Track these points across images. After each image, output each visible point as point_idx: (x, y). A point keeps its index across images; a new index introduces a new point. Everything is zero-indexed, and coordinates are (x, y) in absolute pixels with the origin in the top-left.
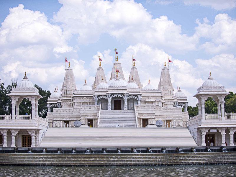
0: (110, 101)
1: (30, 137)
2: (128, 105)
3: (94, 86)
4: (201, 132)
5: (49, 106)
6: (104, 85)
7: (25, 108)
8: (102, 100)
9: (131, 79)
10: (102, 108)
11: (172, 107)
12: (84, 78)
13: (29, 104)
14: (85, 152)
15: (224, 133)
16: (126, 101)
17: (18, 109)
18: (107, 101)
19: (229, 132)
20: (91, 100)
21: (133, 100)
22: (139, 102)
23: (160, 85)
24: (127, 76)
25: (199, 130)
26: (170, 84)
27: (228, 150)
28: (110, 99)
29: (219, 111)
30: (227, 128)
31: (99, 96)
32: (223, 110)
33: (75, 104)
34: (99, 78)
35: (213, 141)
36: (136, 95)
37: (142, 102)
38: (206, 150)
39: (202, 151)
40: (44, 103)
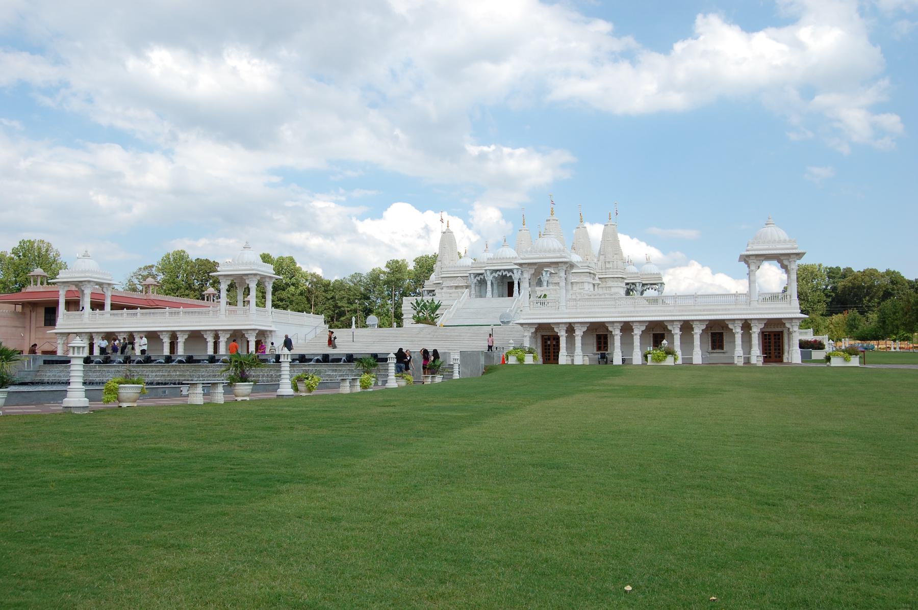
0: (489, 283)
31: (496, 271)
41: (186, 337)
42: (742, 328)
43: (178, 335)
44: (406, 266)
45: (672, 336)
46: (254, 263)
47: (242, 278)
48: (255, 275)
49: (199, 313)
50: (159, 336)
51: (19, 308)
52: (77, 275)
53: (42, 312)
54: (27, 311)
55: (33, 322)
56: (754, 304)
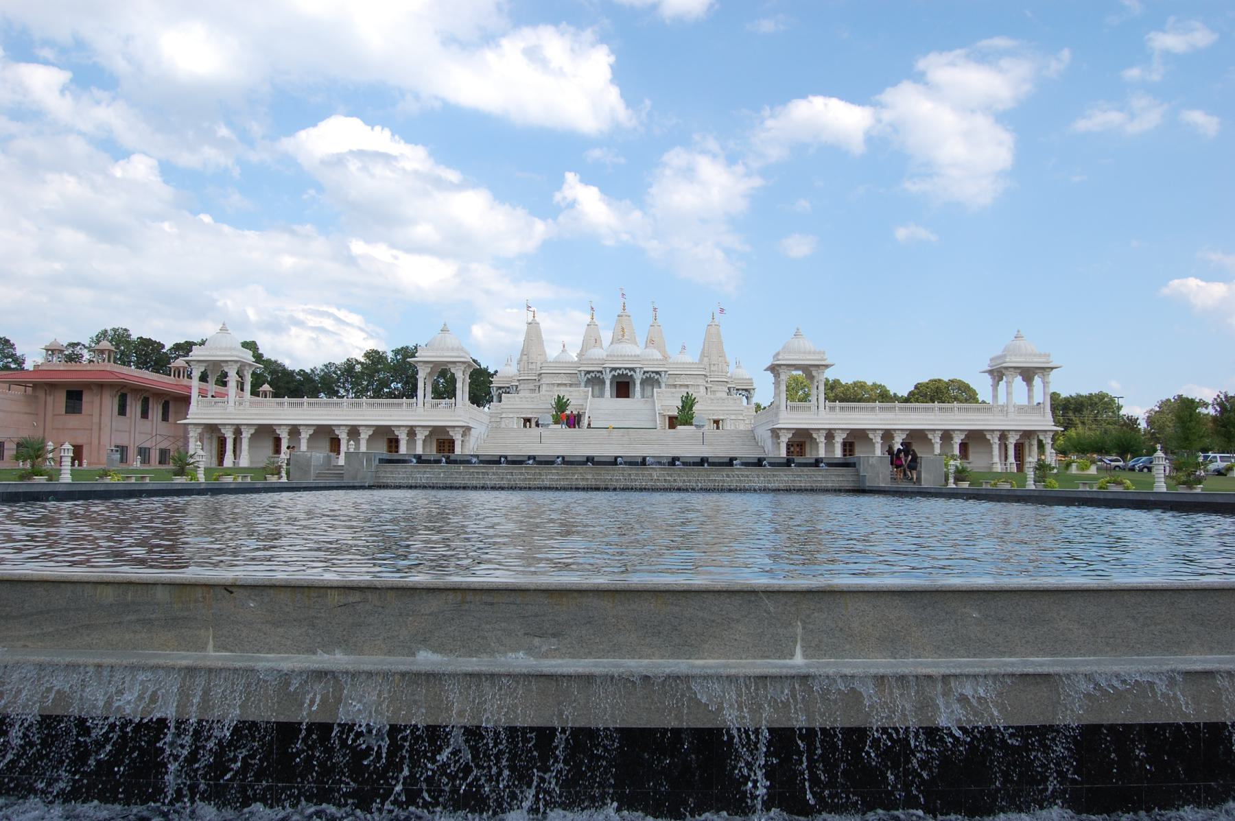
0: (608, 383)
1: (452, 443)
2: (643, 390)
3: (580, 355)
4: (778, 437)
5: (494, 393)
6: (598, 353)
7: (444, 389)
8: (595, 380)
9: (650, 342)
10: (593, 396)
11: (725, 395)
12: (565, 340)
13: (453, 381)
14: (552, 463)
15: (823, 439)
16: (638, 383)
17: (429, 389)
18: (603, 382)
19: (833, 438)
20: (574, 381)
21: (652, 380)
22: (663, 385)
23: (703, 355)
24: (641, 339)
25: (775, 433)
26: (722, 355)
27: (830, 465)
28: (608, 378)
29: (813, 399)
30: (830, 430)
31: (588, 372)
32: (822, 396)
33: (544, 388)
34: (592, 338)
35: (801, 445)
36: (657, 373)
37: (668, 386)
38: (788, 463)
39: (779, 465)
40: (482, 387)
41: (311, 432)
42: (408, 435)
43: (418, 430)
44: (386, 358)
45: (933, 445)
46: (234, 349)
47: (217, 364)
48: (236, 362)
49: (861, 409)
50: (867, 436)
51: (29, 390)
52: (214, 352)
53: (61, 399)
54: (41, 394)
55: (49, 407)
56: (1011, 416)
